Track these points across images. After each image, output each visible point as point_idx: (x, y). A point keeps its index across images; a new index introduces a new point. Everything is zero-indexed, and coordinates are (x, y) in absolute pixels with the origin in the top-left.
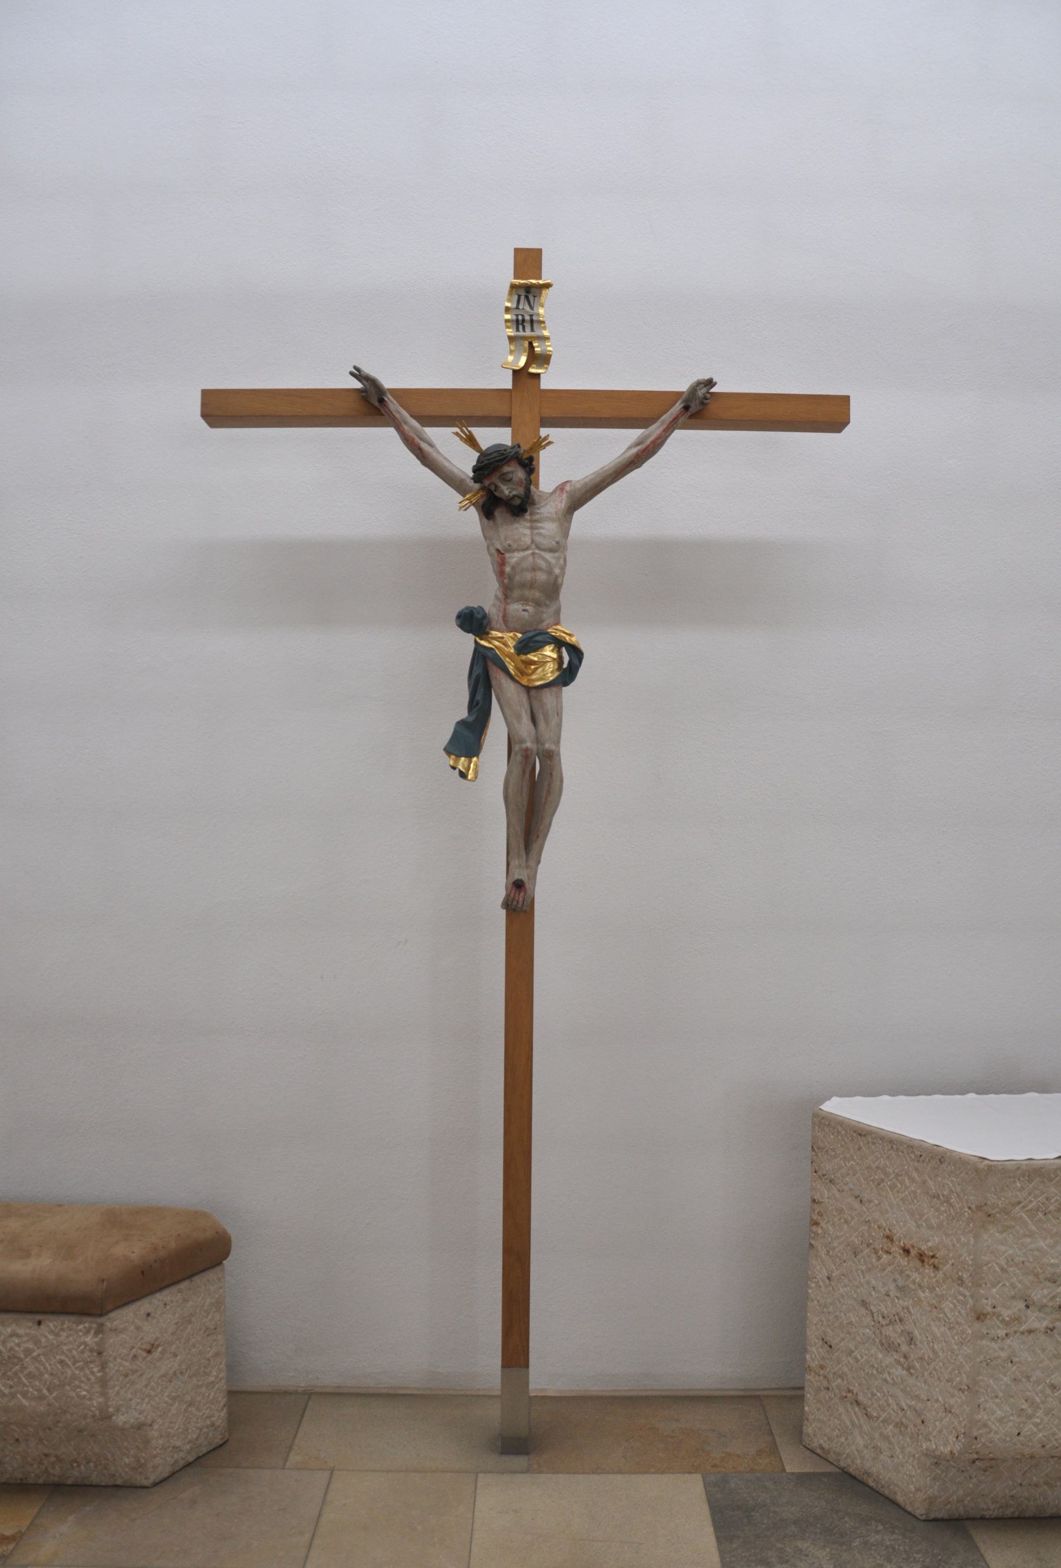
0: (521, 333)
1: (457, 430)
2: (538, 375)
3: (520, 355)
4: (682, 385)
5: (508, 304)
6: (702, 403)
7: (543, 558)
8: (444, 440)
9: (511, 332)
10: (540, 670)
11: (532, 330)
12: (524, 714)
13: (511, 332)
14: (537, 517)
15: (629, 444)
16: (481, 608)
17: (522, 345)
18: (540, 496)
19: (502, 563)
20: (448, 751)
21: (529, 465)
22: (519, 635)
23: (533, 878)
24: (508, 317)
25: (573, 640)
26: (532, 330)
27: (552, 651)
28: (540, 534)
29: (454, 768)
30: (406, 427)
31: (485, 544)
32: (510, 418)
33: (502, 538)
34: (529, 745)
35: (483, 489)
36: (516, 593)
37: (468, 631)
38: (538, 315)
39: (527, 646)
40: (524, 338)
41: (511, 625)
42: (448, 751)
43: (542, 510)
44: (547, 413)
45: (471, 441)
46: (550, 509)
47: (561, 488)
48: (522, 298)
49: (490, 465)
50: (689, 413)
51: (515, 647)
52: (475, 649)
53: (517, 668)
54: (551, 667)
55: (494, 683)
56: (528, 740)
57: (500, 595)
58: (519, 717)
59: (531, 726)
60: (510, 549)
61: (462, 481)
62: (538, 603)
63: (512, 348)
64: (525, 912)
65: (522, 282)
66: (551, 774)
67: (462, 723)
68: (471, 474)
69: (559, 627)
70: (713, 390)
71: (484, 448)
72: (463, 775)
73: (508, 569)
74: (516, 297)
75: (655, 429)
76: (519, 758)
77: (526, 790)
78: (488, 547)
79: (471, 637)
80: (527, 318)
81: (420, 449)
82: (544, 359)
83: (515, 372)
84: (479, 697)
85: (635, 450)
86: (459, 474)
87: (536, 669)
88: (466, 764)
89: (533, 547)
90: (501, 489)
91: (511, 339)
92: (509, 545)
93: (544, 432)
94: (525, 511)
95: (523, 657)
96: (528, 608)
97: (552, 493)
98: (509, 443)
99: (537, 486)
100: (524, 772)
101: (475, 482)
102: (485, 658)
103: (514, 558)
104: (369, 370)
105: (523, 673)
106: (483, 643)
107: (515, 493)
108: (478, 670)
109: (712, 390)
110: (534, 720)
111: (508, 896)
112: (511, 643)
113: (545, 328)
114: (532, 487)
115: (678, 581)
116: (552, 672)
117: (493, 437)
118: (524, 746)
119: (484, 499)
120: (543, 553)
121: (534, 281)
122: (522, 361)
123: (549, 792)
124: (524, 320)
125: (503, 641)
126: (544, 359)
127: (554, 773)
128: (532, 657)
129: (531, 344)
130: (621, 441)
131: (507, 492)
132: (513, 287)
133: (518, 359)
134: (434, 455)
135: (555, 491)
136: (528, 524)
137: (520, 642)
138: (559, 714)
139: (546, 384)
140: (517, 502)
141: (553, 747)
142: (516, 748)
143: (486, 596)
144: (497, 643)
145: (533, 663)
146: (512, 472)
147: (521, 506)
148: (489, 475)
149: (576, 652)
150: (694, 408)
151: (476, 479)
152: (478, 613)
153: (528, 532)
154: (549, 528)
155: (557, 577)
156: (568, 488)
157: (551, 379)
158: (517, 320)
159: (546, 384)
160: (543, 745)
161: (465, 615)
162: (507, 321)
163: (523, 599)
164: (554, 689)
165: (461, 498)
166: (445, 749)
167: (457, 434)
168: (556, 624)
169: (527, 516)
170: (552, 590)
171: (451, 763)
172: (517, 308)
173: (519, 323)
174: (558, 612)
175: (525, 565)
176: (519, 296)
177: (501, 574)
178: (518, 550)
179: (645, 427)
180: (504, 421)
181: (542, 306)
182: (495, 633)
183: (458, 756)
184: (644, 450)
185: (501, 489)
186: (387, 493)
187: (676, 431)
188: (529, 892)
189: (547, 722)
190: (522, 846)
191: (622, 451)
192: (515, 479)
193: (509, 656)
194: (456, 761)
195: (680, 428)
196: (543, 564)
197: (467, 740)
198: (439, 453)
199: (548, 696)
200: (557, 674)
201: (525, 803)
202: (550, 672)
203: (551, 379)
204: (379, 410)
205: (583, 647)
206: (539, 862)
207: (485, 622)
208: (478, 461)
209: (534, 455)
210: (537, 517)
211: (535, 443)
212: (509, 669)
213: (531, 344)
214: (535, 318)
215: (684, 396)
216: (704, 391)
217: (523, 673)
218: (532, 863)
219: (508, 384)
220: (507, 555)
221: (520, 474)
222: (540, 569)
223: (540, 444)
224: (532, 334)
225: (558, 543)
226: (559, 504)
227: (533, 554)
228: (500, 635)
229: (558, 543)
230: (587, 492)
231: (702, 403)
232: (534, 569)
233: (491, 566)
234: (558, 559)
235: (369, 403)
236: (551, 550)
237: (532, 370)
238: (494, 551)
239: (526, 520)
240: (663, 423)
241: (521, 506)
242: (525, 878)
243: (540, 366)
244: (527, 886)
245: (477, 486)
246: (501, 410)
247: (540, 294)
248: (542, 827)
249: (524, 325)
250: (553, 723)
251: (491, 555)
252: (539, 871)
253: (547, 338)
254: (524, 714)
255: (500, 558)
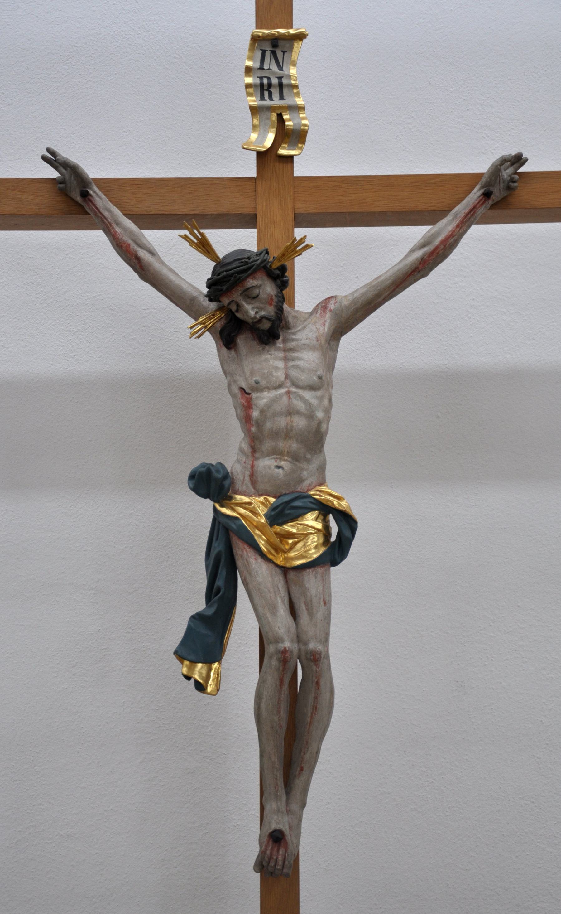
0: (267, 102)
1: (186, 232)
2: (291, 158)
3: (266, 132)
4: (481, 165)
5: (250, 63)
6: (509, 188)
7: (301, 398)
8: (168, 246)
9: (253, 101)
10: (300, 545)
11: (282, 98)
12: (280, 604)
13: (253, 101)
14: (292, 344)
15: (410, 246)
16: (220, 464)
17: (269, 118)
18: (295, 317)
19: (248, 406)
20: (180, 655)
21: (281, 277)
22: (272, 500)
23: (297, 827)
24: (249, 80)
25: (343, 505)
26: (282, 98)
27: (316, 519)
28: (297, 367)
29: (188, 678)
30: (118, 230)
31: (225, 381)
32: (256, 215)
33: (248, 373)
34: (287, 644)
35: (221, 309)
36: (268, 445)
37: (205, 497)
38: (289, 77)
39: (281, 514)
40: (270, 109)
41: (261, 487)
42: (180, 655)
43: (299, 336)
44: (303, 207)
45: (204, 247)
46: (308, 333)
47: (323, 306)
48: (268, 54)
49: (229, 277)
50: (490, 202)
51: (266, 516)
52: (214, 519)
53: (269, 542)
54: (314, 540)
55: (239, 563)
56: (286, 638)
57: (246, 447)
58: (273, 609)
59: (290, 620)
60: (257, 387)
61: (193, 300)
62: (295, 458)
63: (256, 122)
64: (287, 875)
65: (266, 32)
66: (318, 683)
67: (197, 618)
68: (205, 290)
69: (323, 488)
70: (522, 169)
71: (221, 256)
72: (200, 687)
73: (255, 414)
74: (259, 54)
75: (446, 225)
76: (275, 663)
77: (284, 707)
78: (229, 386)
79: (208, 503)
80: (275, 81)
81: (138, 258)
82: (298, 137)
83: (261, 155)
84: (220, 582)
85: (419, 254)
86: (190, 290)
87: (295, 544)
88: (204, 672)
89: (288, 384)
90: (244, 308)
91: (254, 110)
92: (257, 383)
93: (299, 233)
94: (277, 337)
95: (278, 529)
96: (282, 463)
97: (311, 314)
98: (254, 249)
99: (292, 305)
100: (281, 681)
101: (211, 300)
102: (227, 530)
103: (263, 399)
104: (66, 153)
105: (277, 550)
106: (224, 510)
107: (262, 313)
108: (218, 547)
109: (521, 170)
110: (293, 611)
111: (262, 853)
112: (262, 510)
113: (298, 95)
114: (285, 306)
115: (475, 424)
116: (316, 547)
117: (233, 241)
118: (281, 646)
119: (223, 322)
120: (301, 392)
121: (282, 31)
122: (269, 141)
123: (315, 708)
124: (270, 85)
125: (251, 508)
126: (298, 137)
127: (322, 683)
128: (289, 528)
129: (280, 116)
130: (402, 241)
131: (252, 313)
132: (255, 39)
133: (263, 138)
134: (157, 266)
135: (315, 310)
136: (281, 355)
137: (273, 508)
138: (327, 603)
139: (300, 169)
140: (266, 325)
141: (320, 647)
142: (270, 649)
143: (228, 451)
144: (242, 511)
145: (290, 535)
146: (259, 287)
147: (272, 331)
148: (229, 290)
149: (347, 521)
150: (498, 193)
151: (211, 297)
152: (218, 471)
153: (281, 364)
154: (309, 359)
155: (320, 423)
156: (332, 306)
157: (308, 163)
158: (262, 85)
159: (300, 169)
160: (306, 644)
161: (201, 474)
162: (248, 86)
163: (277, 453)
164: (320, 570)
165: (192, 322)
166: (176, 653)
167: (185, 237)
168: (322, 483)
169: (279, 344)
170: (314, 440)
171: (185, 670)
172: (261, 68)
173: (264, 89)
174: (322, 469)
175: (278, 408)
176: (264, 52)
177: (246, 420)
178: (269, 389)
179: (432, 222)
180: (247, 220)
181: (294, 65)
182: (240, 498)
183: (194, 662)
184: (432, 253)
185: (244, 308)
186: (94, 317)
187: (474, 227)
188: (291, 847)
189: (311, 614)
190: (281, 783)
191: (403, 256)
192: (263, 296)
193: (259, 527)
194: (191, 669)
195: (478, 223)
196: (300, 406)
197: (205, 639)
198: (162, 263)
199: (311, 580)
200: (322, 550)
201: (284, 725)
202: (313, 547)
203: (308, 163)
204: (82, 207)
205: (356, 513)
206: (304, 805)
207: (227, 483)
208: (214, 273)
209: (287, 264)
210: (292, 344)
211: (287, 248)
212: (257, 550)
213: (280, 116)
214: (285, 81)
215: (484, 180)
216: (510, 170)
217: (277, 550)
218: (294, 807)
219: (249, 169)
220: (254, 395)
221: (269, 289)
222: (298, 413)
223: (295, 248)
224: (282, 103)
225: (320, 378)
226: (322, 326)
227: (288, 393)
228: (246, 499)
229: (320, 378)
230: (357, 311)
231: (509, 188)
232: (290, 412)
233: (233, 411)
234: (321, 398)
235: (69, 198)
236: (312, 388)
237: (282, 152)
238: (236, 390)
239: (278, 349)
240: (455, 216)
241: (272, 331)
242: (285, 828)
243: (293, 146)
244: (288, 838)
245: (213, 306)
246: (243, 206)
247: (292, 48)
248: (307, 756)
249: (271, 90)
250: (319, 615)
251: (233, 396)
252: (304, 816)
253: (301, 108)
254: (280, 604)
255: (245, 397)
